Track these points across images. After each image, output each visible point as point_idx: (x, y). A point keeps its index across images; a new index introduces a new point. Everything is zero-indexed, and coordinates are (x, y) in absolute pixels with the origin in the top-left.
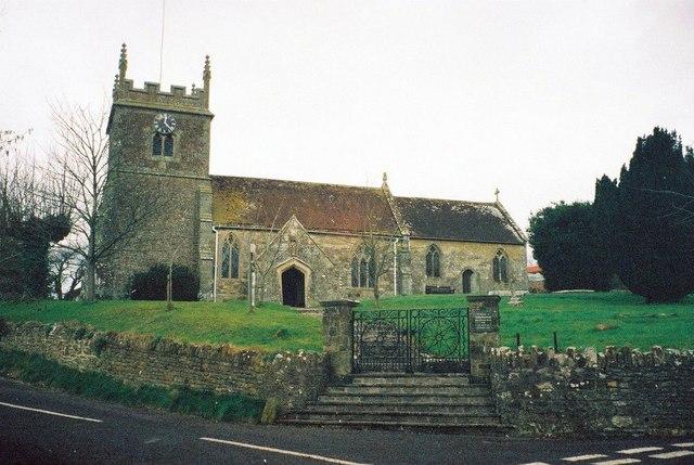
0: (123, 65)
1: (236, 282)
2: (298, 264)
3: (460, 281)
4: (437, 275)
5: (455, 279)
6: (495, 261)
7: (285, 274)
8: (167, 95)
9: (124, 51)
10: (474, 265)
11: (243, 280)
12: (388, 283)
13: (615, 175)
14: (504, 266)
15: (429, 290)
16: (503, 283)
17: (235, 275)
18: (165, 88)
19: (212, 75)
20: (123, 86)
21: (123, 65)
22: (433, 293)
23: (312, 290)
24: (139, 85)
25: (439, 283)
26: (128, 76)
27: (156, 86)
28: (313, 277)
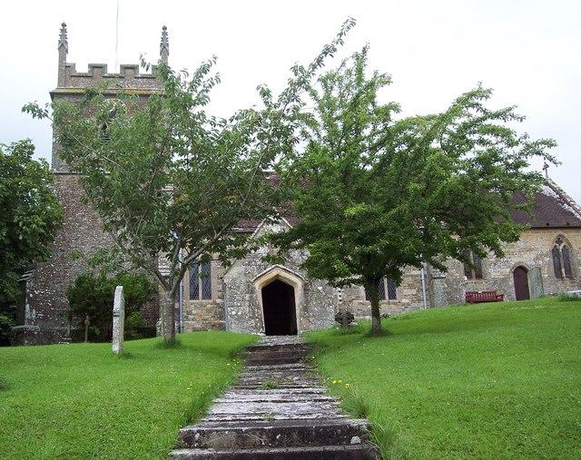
0: (63, 48)
1: (208, 303)
2: (283, 274)
3: (511, 282)
4: (479, 276)
5: (504, 280)
6: (555, 252)
7: (265, 290)
8: (85, 76)
9: (165, 34)
10: (527, 260)
11: (219, 301)
12: (414, 292)
13: (221, 108)
14: (567, 259)
15: (472, 299)
16: (568, 281)
17: (208, 295)
18: (113, 69)
19: (171, 49)
20: (66, 71)
21: (63, 48)
22: (476, 302)
23: (305, 309)
24: (82, 69)
25: (481, 287)
26: (69, 60)
27: (102, 67)
28: (306, 290)
